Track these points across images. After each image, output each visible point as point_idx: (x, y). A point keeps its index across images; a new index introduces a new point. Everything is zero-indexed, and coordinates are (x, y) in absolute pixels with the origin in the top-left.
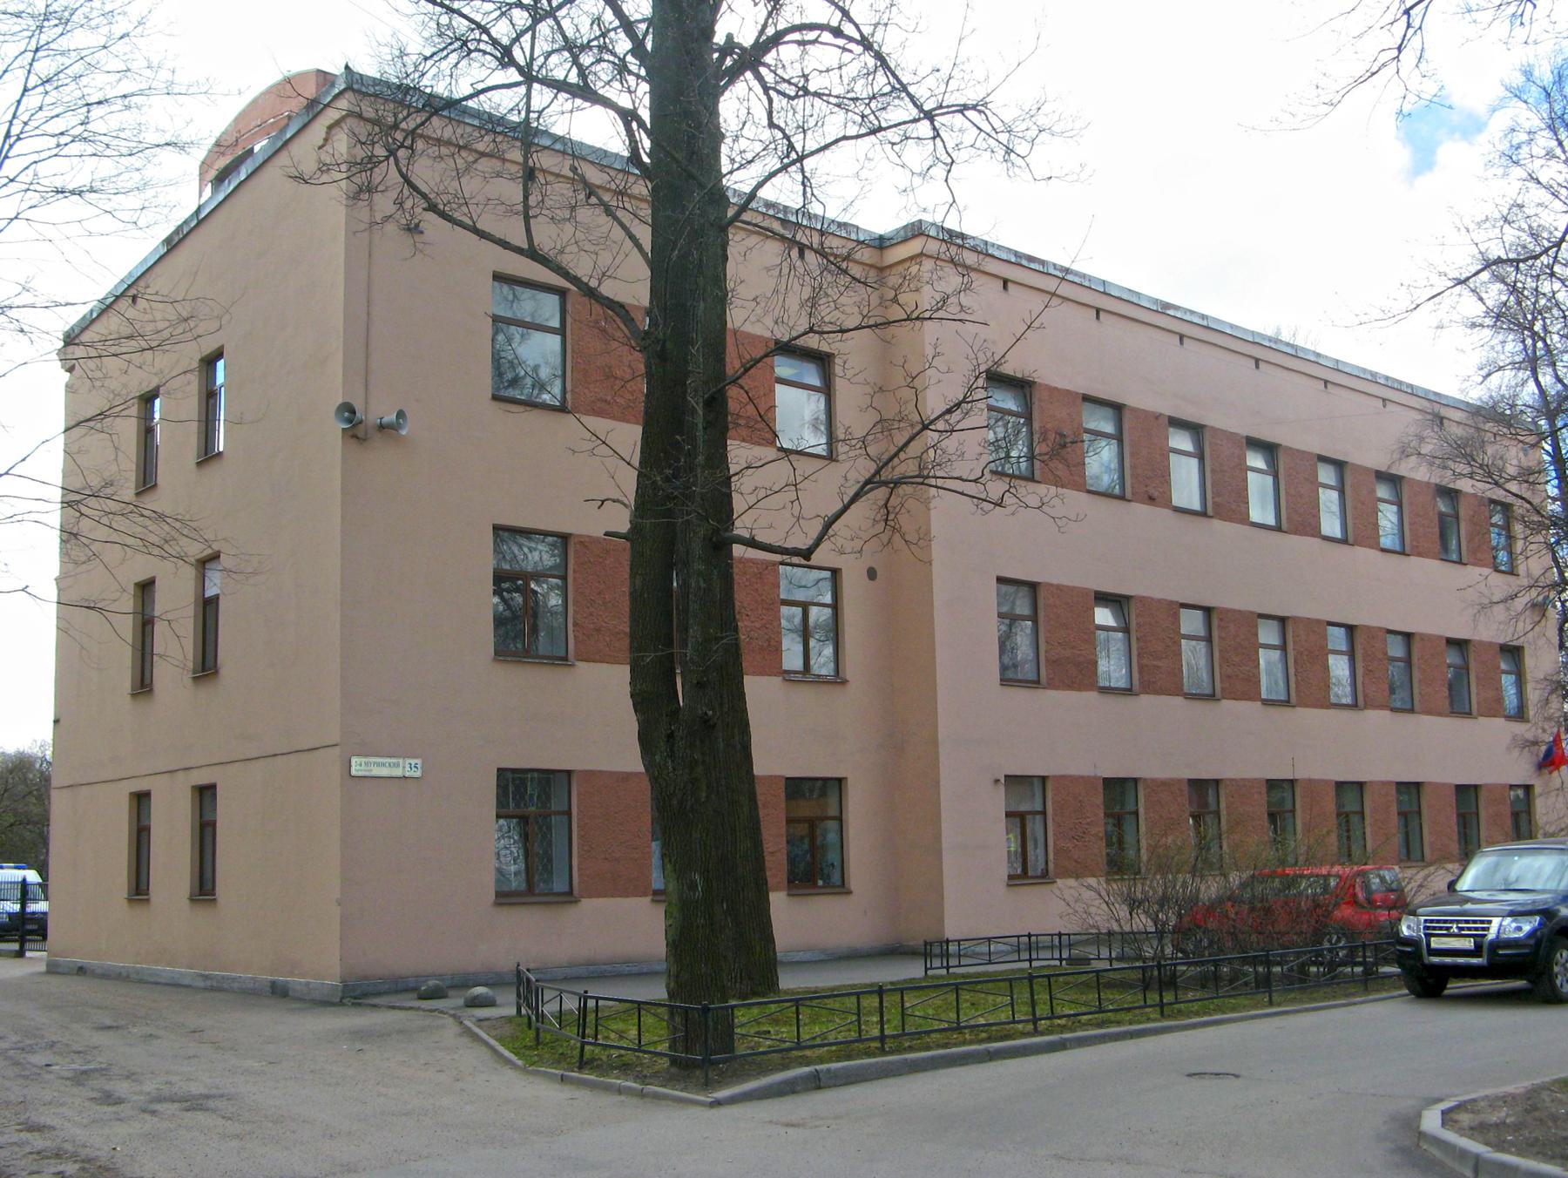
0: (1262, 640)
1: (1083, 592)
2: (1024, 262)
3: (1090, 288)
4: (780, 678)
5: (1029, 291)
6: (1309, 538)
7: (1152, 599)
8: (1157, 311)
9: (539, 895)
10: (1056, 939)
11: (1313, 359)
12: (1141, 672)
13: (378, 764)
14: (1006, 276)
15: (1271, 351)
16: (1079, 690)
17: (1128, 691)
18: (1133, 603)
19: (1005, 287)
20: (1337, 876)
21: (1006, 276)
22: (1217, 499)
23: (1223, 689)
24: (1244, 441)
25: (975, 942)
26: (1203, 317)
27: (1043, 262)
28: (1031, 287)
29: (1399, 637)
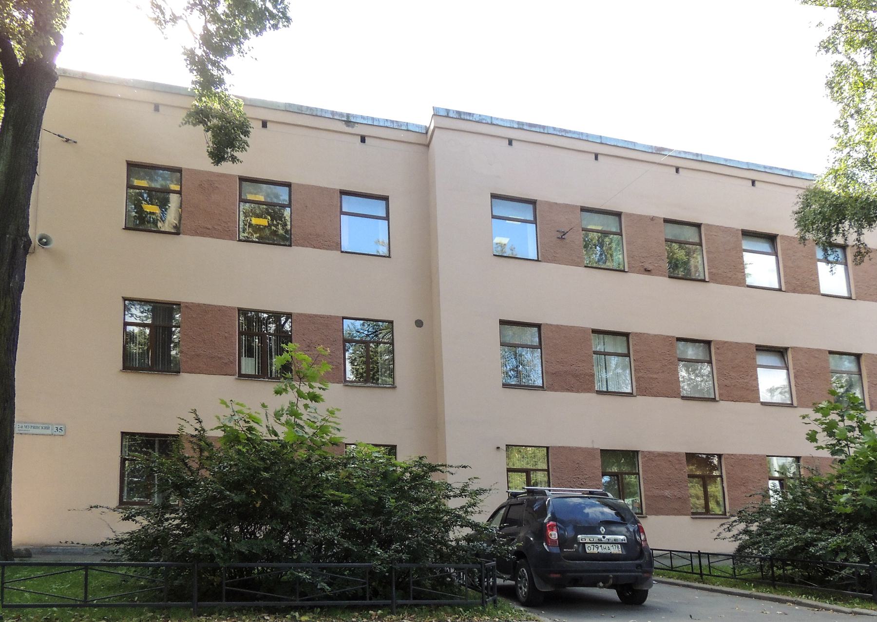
0: (759, 363)
1: (746, 346)
2: (525, 127)
3: (588, 141)
4: (342, 384)
5: (726, 177)
6: (808, 295)
7: (649, 334)
8: (652, 153)
9: (712, 515)
10: (696, 562)
11: (763, 170)
12: (637, 381)
13: (34, 428)
14: (509, 137)
15: (766, 174)
16: (578, 392)
17: (542, 388)
18: (790, 352)
19: (596, 158)
20: (600, 534)
21: (754, 178)
22: (713, 270)
23: (720, 395)
24: (741, 232)
25: (71, 568)
26: (697, 155)
27: (544, 127)
28: (692, 169)
29: (853, 357)
